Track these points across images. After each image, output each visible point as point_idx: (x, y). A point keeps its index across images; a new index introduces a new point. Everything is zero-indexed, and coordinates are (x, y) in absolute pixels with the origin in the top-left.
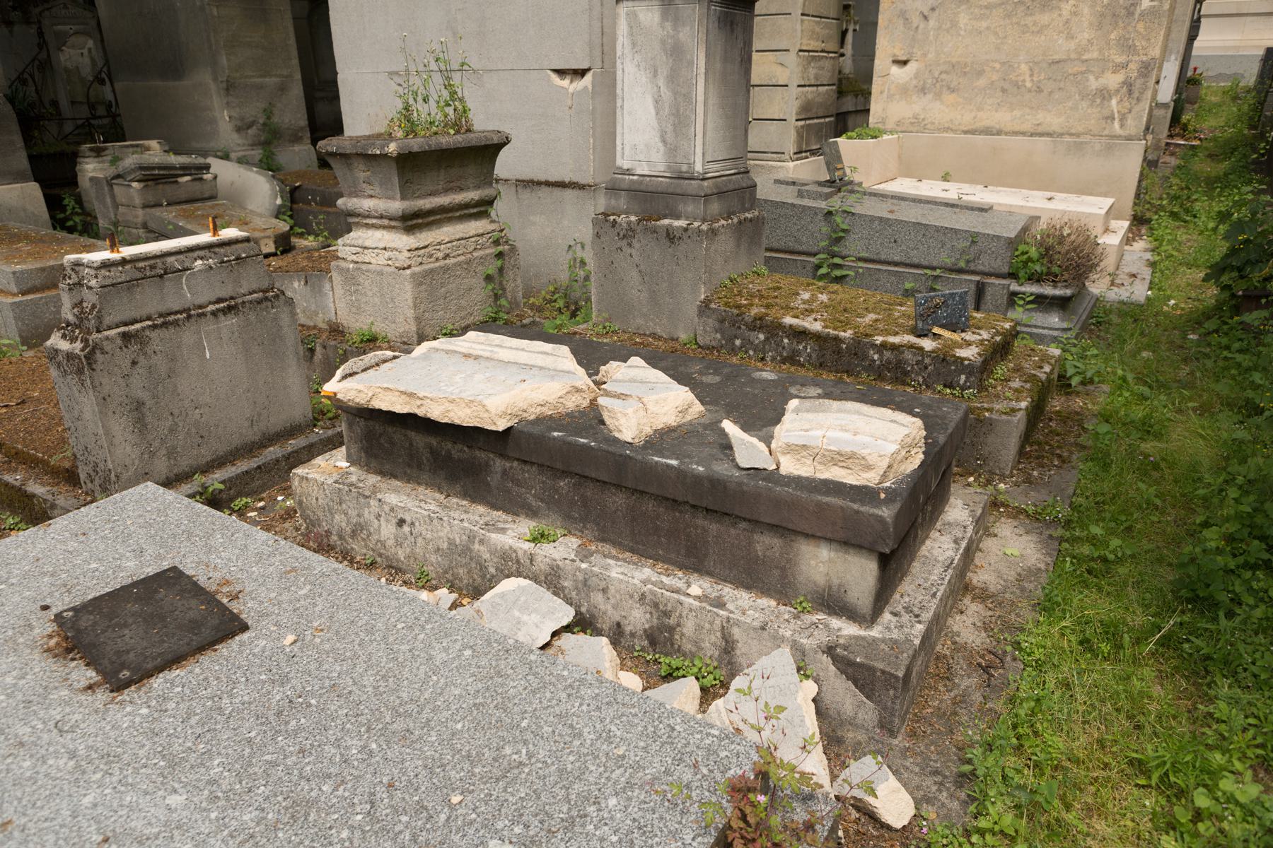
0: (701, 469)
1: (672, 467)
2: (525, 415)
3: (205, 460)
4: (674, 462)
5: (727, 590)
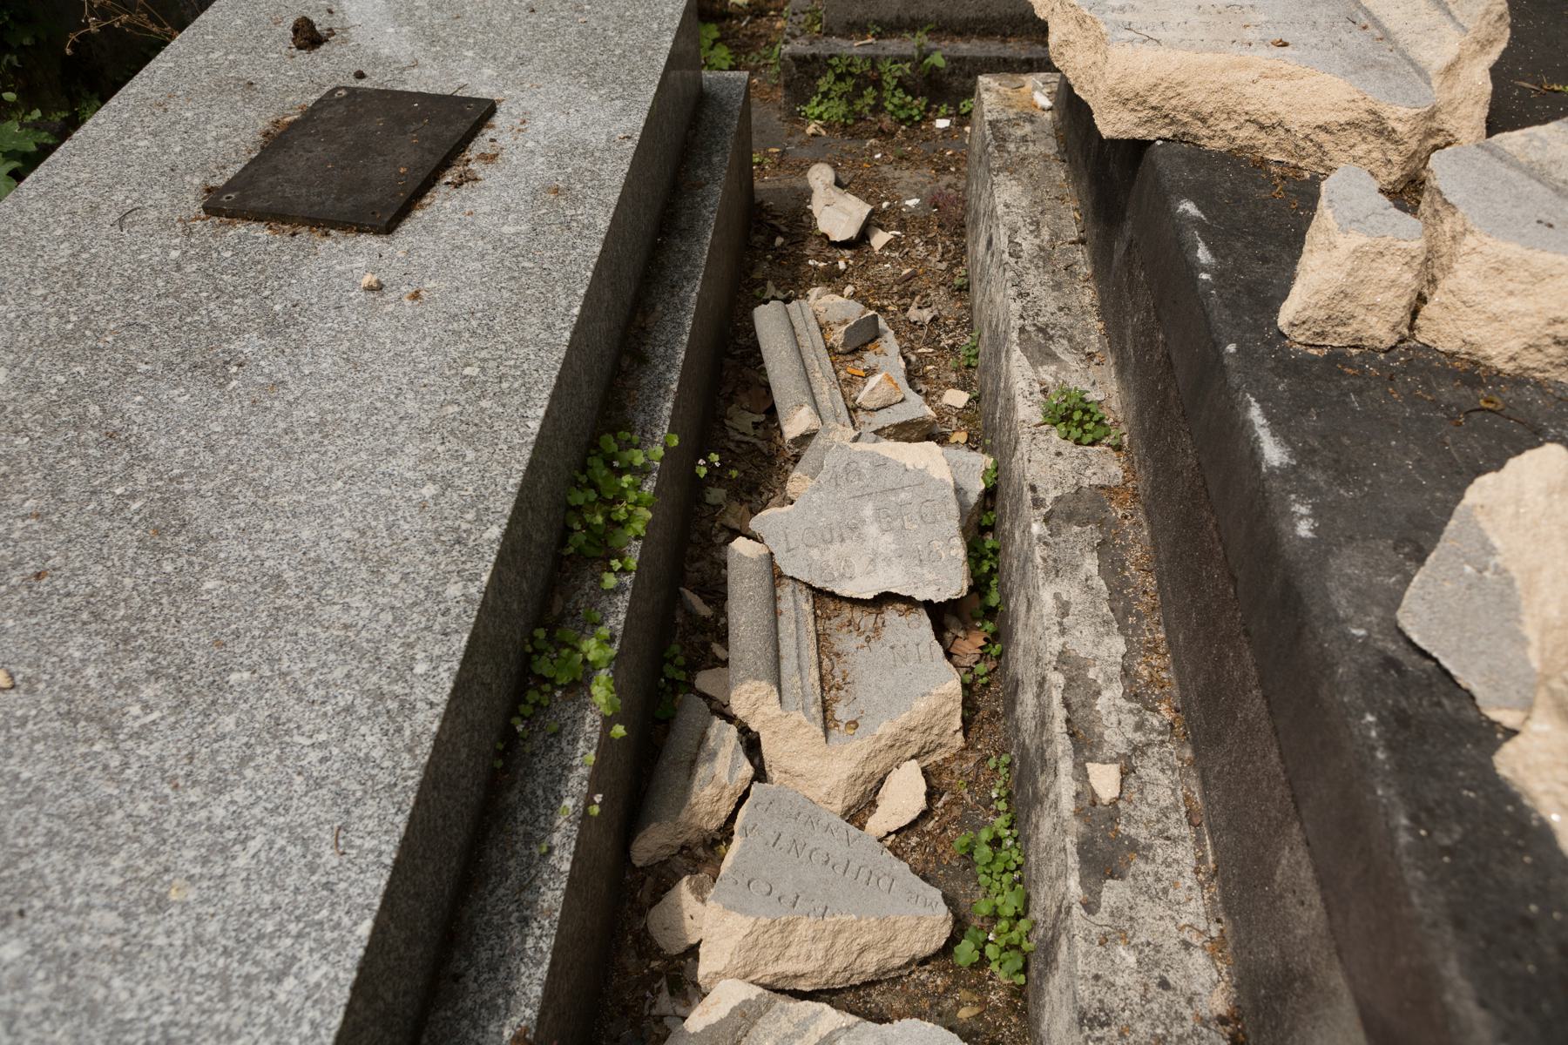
0: (1304, 529)
1: (1255, 454)
2: (1197, 128)
3: (964, 15)
4: (1273, 453)
5: (1185, 854)
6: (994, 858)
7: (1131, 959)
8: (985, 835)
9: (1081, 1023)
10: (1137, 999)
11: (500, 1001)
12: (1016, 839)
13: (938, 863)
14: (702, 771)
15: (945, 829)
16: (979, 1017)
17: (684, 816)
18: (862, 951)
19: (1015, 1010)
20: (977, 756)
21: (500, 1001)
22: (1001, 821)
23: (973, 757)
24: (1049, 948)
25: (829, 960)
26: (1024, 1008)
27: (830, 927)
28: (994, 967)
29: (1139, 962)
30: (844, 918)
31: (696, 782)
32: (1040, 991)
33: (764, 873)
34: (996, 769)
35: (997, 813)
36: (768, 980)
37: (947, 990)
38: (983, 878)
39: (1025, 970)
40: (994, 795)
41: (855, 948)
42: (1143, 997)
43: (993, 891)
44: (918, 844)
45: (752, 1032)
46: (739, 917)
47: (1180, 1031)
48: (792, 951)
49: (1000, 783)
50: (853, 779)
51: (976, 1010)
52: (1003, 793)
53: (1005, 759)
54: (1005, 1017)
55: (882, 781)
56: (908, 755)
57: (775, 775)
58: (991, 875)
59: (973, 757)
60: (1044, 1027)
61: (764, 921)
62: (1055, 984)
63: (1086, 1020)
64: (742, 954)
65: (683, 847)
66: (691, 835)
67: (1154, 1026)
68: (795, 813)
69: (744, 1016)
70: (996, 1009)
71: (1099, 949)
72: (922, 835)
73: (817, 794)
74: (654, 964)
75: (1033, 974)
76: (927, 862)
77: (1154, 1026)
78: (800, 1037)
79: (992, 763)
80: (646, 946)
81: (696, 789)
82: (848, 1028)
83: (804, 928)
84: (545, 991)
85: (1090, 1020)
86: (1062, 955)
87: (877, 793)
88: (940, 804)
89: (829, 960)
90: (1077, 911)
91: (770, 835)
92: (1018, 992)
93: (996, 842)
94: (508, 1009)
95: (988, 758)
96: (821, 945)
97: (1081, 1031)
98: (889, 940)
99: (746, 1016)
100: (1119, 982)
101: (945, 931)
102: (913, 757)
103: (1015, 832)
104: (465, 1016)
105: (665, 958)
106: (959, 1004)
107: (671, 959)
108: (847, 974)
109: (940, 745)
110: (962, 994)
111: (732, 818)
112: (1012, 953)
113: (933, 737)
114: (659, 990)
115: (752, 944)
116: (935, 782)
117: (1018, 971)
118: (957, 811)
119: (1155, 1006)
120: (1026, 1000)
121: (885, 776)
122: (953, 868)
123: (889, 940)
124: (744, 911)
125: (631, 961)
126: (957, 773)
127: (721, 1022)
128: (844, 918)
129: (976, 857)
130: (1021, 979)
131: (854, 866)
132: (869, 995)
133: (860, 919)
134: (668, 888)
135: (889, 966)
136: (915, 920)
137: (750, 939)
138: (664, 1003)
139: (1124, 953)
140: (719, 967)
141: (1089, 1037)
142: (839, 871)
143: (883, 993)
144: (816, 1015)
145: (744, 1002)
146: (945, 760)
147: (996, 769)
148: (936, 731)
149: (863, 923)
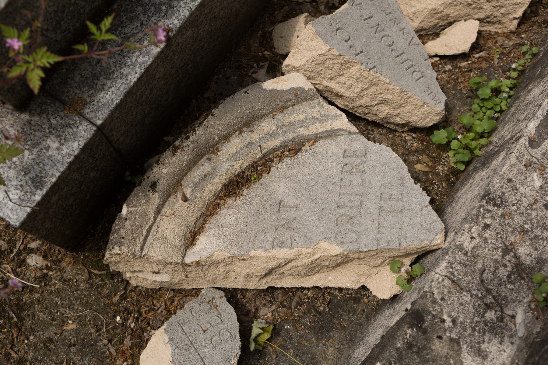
6: (490, 98)
7: (538, 183)
8: (493, 84)
9: (483, 197)
10: (526, 205)
11: (164, 8)
12: (510, 97)
15: (471, 71)
18: (382, 102)
19: (448, 180)
20: (518, 41)
21: (164, 8)
22: (508, 82)
23: (515, 40)
24: (489, 157)
25: (360, 97)
26: (454, 183)
27: (371, 78)
28: (451, 153)
29: (541, 187)
32: (469, 176)
33: (350, 29)
34: (524, 54)
35: (508, 78)
36: (321, 88)
37: (417, 151)
38: (475, 107)
39: (467, 164)
40: (514, 66)
41: (379, 98)
42: (530, 205)
43: (477, 116)
44: (450, 71)
45: (297, 106)
46: (322, 42)
47: (540, 233)
48: (342, 79)
49: (522, 62)
50: (435, 12)
51: (426, 169)
52: (520, 68)
54: (440, 181)
55: (450, 24)
56: (476, 16)
58: (481, 108)
59: (515, 40)
60: (459, 194)
61: (335, 52)
62: (484, 173)
63: (487, 196)
64: (313, 64)
67: (525, 222)
68: (388, 11)
69: (296, 95)
70: (438, 174)
71: (522, 167)
72: (455, 67)
73: (408, 10)
74: (266, 53)
75: (471, 168)
76: (448, 82)
77: (525, 222)
78: (321, 122)
79: (524, 48)
80: (267, 41)
82: (350, 133)
83: (355, 70)
84: (191, 16)
85: (490, 199)
86: (496, 162)
87: (443, 29)
88: (477, 56)
89: (360, 97)
90: (524, 141)
92: (456, 173)
93: (497, 92)
94: (166, 14)
95: (524, 44)
96: (360, 85)
97: (480, 201)
98: (400, 105)
99: (297, 97)
100: (522, 190)
101: (436, 119)
102: (478, 19)
103: (512, 93)
104: (142, 5)
105: (274, 53)
106: (419, 161)
107: (275, 54)
108: (366, 111)
109: (499, 22)
110: (424, 158)
112: (466, 151)
113: (498, 14)
114: (262, 67)
115: (321, 61)
116: (482, 42)
117: (463, 162)
118: (484, 65)
119: (534, 214)
120: (457, 179)
121: (455, 21)
122: (462, 94)
123: (400, 105)
124: (326, 41)
125: (255, 45)
126: (499, 44)
127: (282, 91)
128: (382, 78)
129: (479, 92)
130: (462, 167)
131: (405, 57)
132: (373, 131)
133: (390, 83)
134: (294, 17)
135: (392, 120)
136: (424, 104)
137: (322, 58)
138: (262, 72)
139: (535, 178)
140: (297, 65)
141: (483, 206)
142: (394, 54)
143: (381, 134)
144: (336, 116)
145: (300, 88)
146: (496, 33)
147: (524, 54)
148: (503, 11)
149: (391, 87)
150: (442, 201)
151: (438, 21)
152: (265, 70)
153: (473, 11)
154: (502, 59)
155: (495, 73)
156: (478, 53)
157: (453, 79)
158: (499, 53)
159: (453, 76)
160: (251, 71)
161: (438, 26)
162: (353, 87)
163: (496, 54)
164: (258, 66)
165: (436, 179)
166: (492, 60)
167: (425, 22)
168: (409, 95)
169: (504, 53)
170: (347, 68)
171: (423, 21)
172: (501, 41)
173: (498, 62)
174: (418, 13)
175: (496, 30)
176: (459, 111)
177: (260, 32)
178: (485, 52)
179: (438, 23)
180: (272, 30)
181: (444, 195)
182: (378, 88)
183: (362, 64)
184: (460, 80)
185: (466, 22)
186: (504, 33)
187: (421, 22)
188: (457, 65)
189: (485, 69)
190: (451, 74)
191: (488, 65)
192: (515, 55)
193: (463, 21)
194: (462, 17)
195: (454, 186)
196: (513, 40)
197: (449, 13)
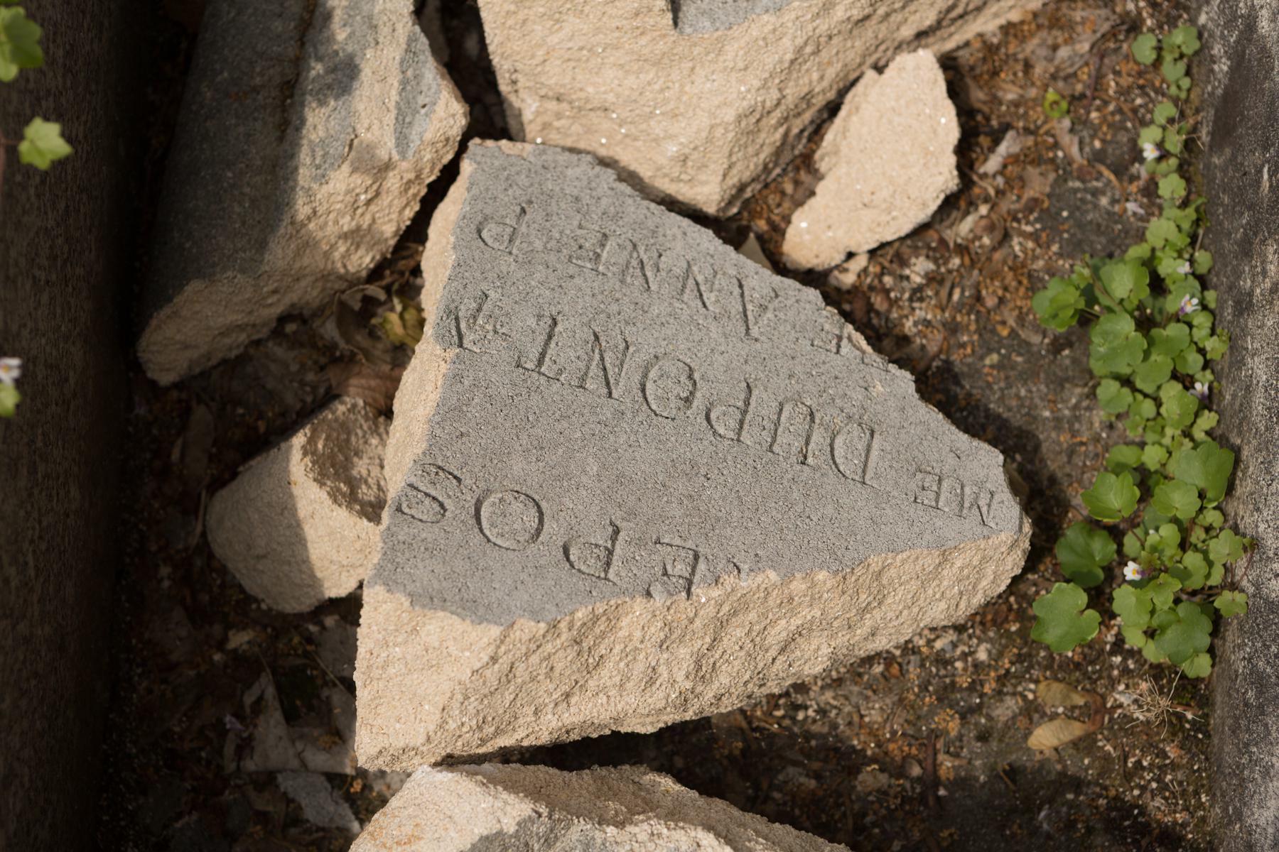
13: (986, 329)
14: (319, 122)
15: (1006, 236)
16: (1084, 744)
17: (278, 255)
26: (1200, 725)
30: (746, 583)
31: (304, 156)
33: (518, 466)
44: (931, 279)
50: (751, 122)
51: (1077, 729)
53: (1181, 37)
54: (1152, 747)
55: (833, 109)
56: (907, 32)
57: (527, 105)
65: (283, 319)
66: (307, 293)
74: (240, 639)
79: (1144, 48)
80: (214, 593)
81: (304, 175)
88: (992, 164)
89: (701, 672)
91: (526, 326)
106: (1033, 712)
107: (282, 625)
111: (416, 232)
124: (472, 608)
131: (764, 403)
146: (1008, 29)
150: (1203, 820)
151: (782, 130)
152: (278, 715)
153: (883, 27)
154: (1086, 122)
155: (1096, 193)
156: (992, 149)
157: (959, 308)
158: (1064, 105)
159: (956, 296)
160: (229, 750)
161: (791, 139)
162: (662, 670)
163: (1056, 114)
164: (239, 716)
165: (1134, 747)
166: (1056, 146)
167: (739, 166)
168: (875, 567)
169: (1083, 96)
170: (603, 635)
171: (730, 167)
172: (1043, 52)
173: (1081, 143)
174: (695, 156)
175: (1002, 21)
176: (1058, 421)
177: (165, 571)
178: (1010, 134)
179: (786, 135)
180: (204, 534)
181: (1197, 793)
182: (752, 616)
183: (648, 594)
184: (991, 302)
185: (889, 72)
186: (1035, 15)
187: (725, 176)
188: (943, 242)
189: (1049, 196)
190: (944, 293)
191: (1052, 176)
192: (1126, 81)
193: (870, 74)
194: (860, 65)
195: (1208, 735)
196: (1084, 21)
197: (806, 90)
